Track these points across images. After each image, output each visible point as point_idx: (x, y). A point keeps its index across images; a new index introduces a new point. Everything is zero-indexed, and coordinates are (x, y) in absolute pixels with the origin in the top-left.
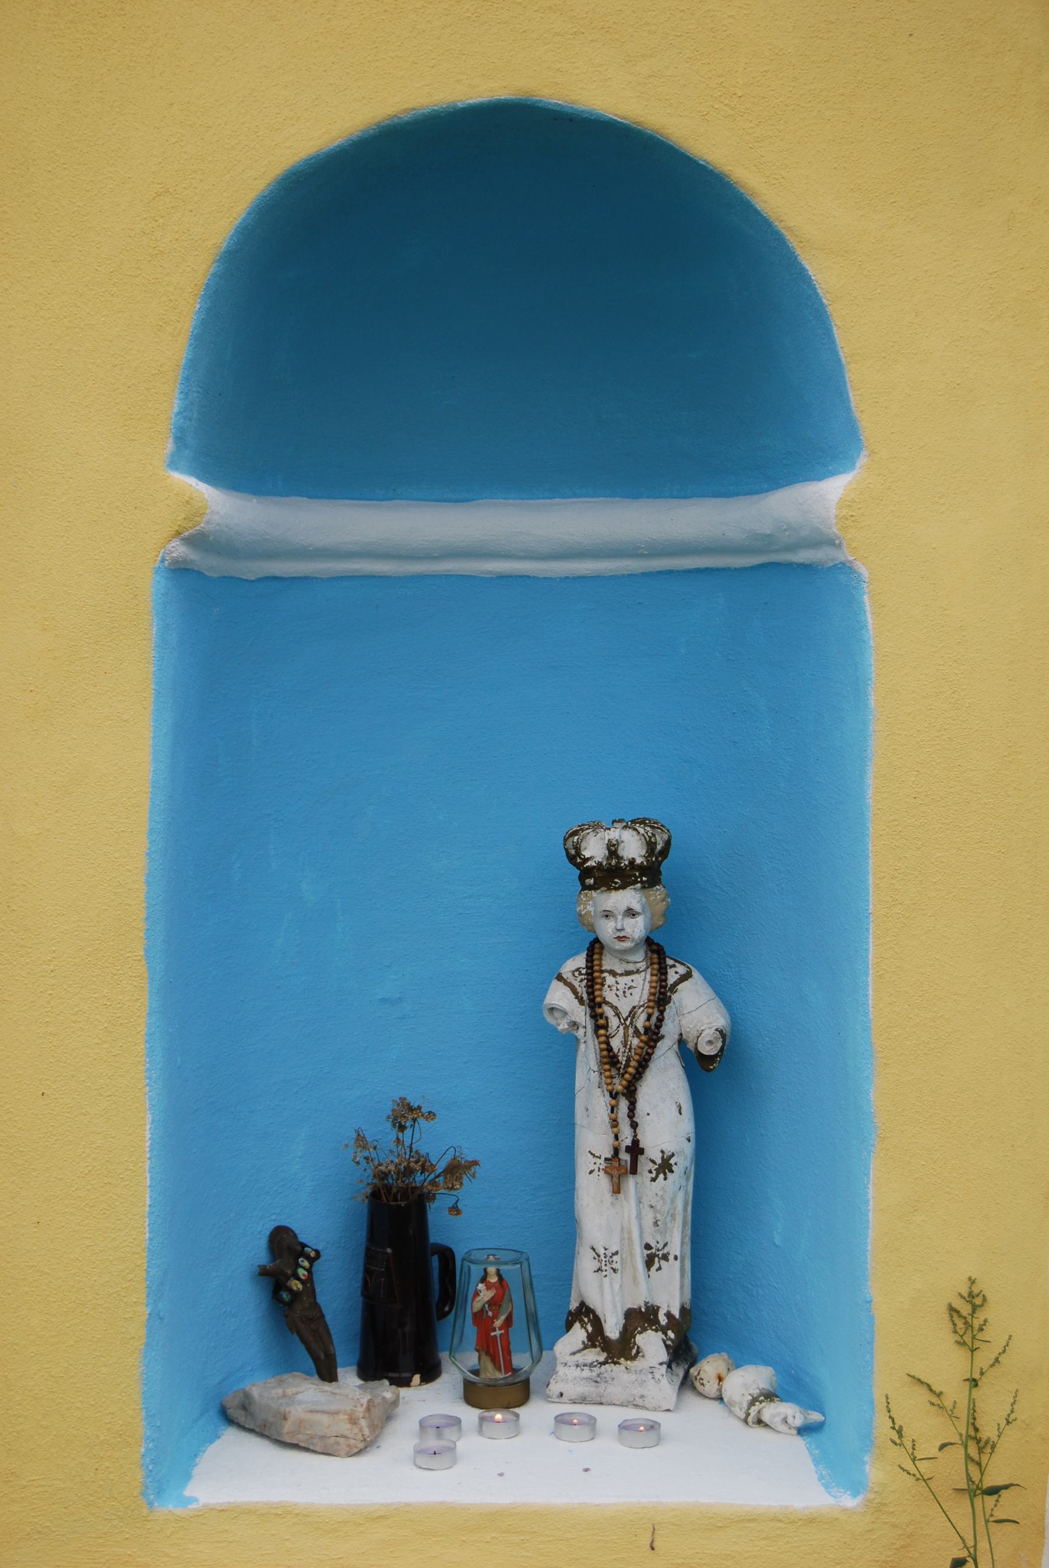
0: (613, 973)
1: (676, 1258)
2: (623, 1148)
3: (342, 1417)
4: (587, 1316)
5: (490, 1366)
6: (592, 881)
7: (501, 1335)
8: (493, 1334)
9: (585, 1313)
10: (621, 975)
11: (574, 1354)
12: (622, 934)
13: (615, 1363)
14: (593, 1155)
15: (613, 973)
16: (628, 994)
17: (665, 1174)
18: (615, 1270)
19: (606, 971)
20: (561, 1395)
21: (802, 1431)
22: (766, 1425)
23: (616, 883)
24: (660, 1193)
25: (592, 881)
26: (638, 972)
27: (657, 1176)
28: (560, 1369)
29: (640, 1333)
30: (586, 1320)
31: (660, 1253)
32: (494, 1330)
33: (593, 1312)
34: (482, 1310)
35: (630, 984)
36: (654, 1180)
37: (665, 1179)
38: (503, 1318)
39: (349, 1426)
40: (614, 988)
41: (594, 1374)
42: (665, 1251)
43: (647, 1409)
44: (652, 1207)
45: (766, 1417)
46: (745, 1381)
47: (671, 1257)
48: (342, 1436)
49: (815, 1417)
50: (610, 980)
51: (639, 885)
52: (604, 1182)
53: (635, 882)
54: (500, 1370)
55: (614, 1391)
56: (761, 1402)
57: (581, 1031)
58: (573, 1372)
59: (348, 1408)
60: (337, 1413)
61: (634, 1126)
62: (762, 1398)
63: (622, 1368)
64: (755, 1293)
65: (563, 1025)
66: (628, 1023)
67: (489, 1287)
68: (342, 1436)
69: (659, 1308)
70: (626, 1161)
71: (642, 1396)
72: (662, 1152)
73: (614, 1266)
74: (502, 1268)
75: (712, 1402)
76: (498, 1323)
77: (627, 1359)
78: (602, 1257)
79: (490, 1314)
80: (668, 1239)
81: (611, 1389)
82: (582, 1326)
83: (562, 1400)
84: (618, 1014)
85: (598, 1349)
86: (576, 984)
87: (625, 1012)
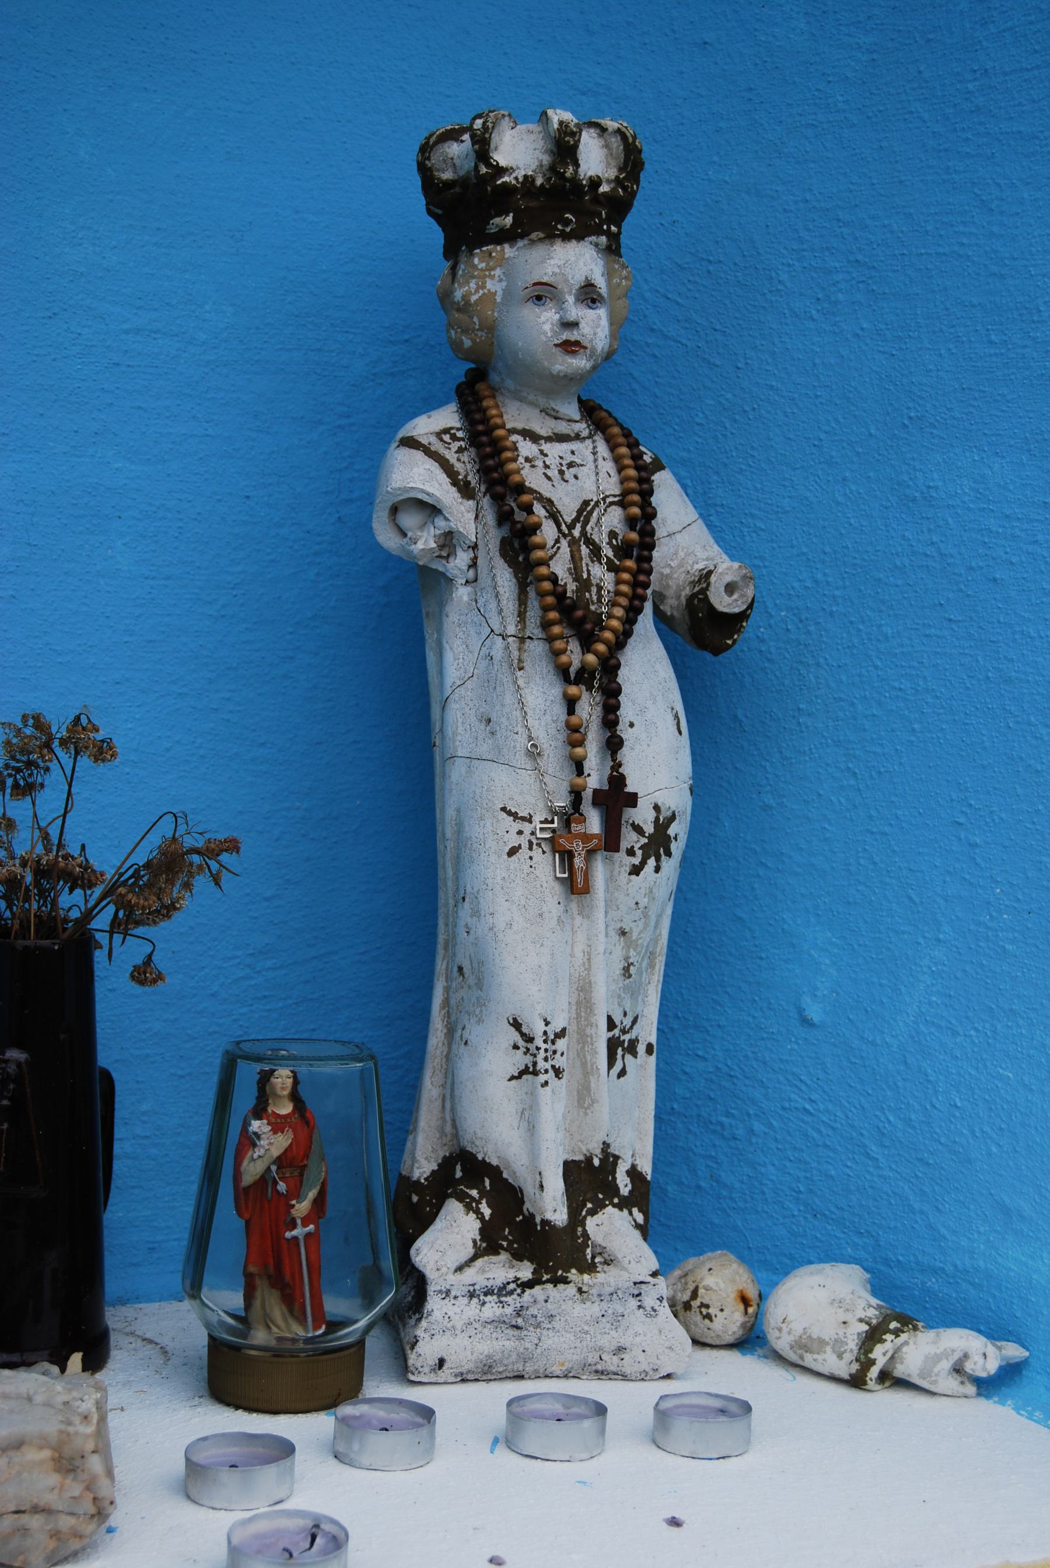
0: (530, 435)
1: (649, 1049)
2: (587, 795)
3: (33, 1455)
4: (478, 1185)
5: (277, 1311)
6: (509, 220)
7: (308, 1236)
8: (288, 1235)
9: (468, 1172)
10: (549, 439)
11: (460, 1269)
12: (573, 336)
13: (556, 1281)
14: (515, 816)
15: (530, 435)
16: (569, 474)
17: (658, 859)
18: (558, 1072)
19: (514, 431)
20: (441, 1362)
21: (986, 1386)
22: (903, 1384)
23: (568, 222)
24: (644, 902)
25: (509, 220)
26: (577, 437)
27: (643, 863)
28: (434, 1303)
29: (593, 1213)
30: (474, 1193)
31: (626, 1037)
32: (293, 1225)
33: (494, 1172)
34: (264, 1181)
35: (570, 458)
36: (636, 870)
37: (657, 869)
38: (312, 1194)
39: (54, 1479)
40: (539, 463)
41: (509, 1310)
42: (632, 1035)
43: (625, 1378)
44: (623, 933)
45: (909, 1366)
46: (823, 1301)
47: (641, 1048)
48: (36, 1509)
49: (1014, 1351)
50: (526, 448)
51: (603, 239)
52: (544, 867)
53: (599, 232)
54: (302, 1321)
55: (559, 1343)
56: (897, 1333)
57: (462, 559)
58: (462, 1311)
59: (52, 1427)
60: (18, 1444)
61: (613, 744)
62: (893, 1325)
63: (571, 1290)
64: (740, 1132)
65: (425, 541)
66: (576, 532)
67: (278, 1125)
68: (36, 1509)
69: (617, 1158)
70: (595, 822)
71: (620, 1350)
72: (657, 808)
73: (559, 1062)
74: (303, 1070)
75: (723, 1353)
76: (302, 1207)
77: (581, 1271)
78: (539, 1042)
79: (282, 1187)
80: (639, 1010)
81: (550, 1340)
82: (468, 1208)
83: (445, 1374)
84: (554, 515)
85: (504, 1256)
86: (451, 456)
87: (569, 511)
